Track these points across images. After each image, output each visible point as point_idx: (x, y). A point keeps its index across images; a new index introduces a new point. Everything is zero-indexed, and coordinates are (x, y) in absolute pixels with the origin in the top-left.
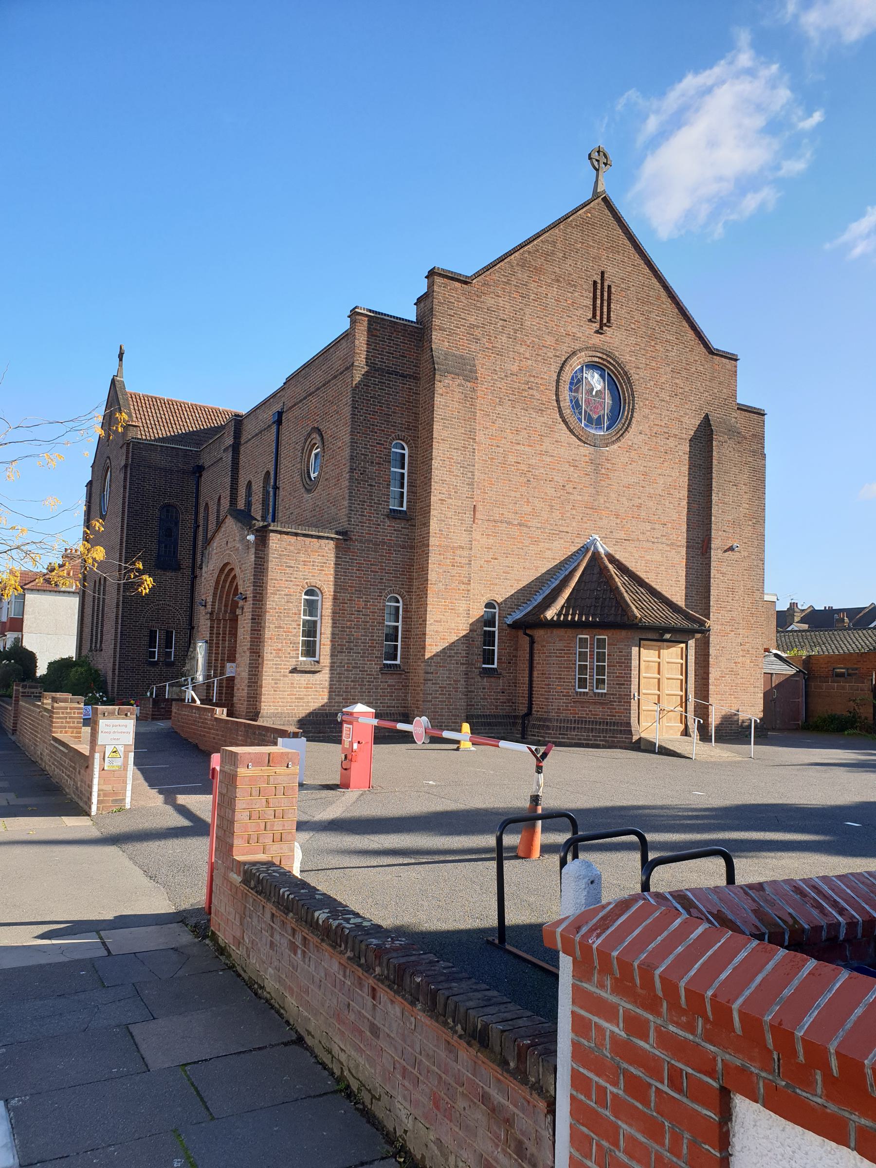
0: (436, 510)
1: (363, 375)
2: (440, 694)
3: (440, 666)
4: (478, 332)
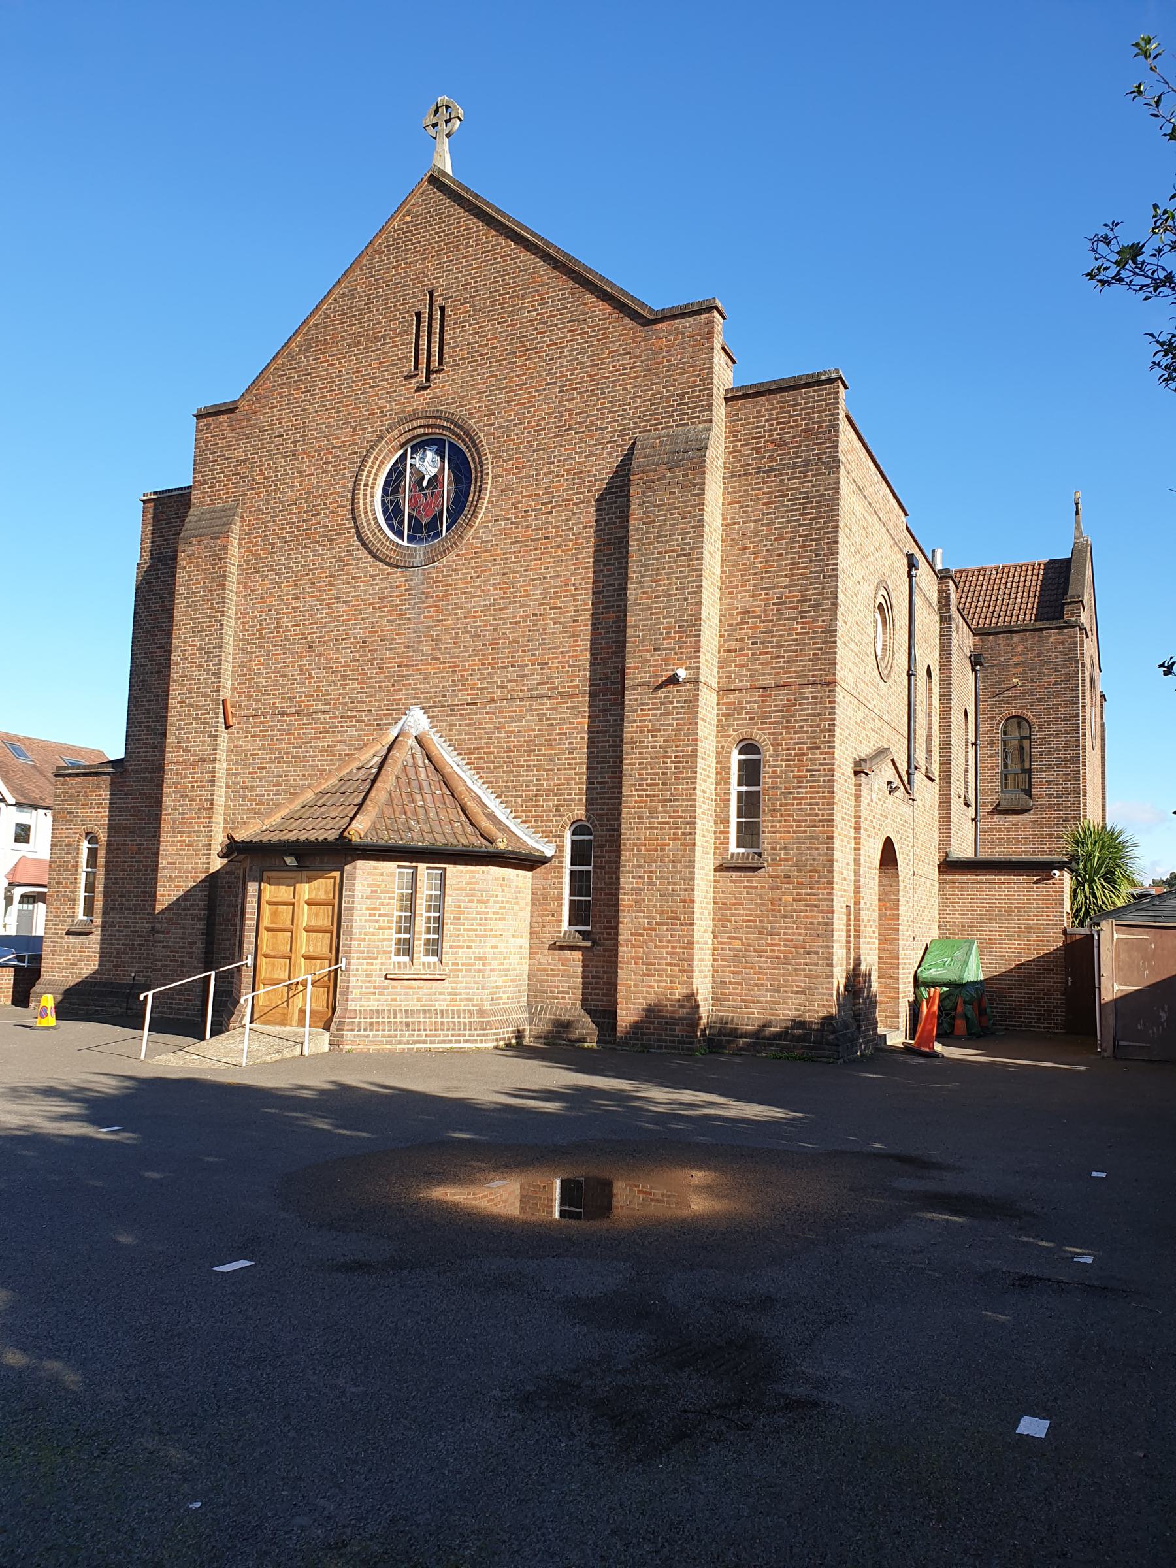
0: (175, 716)
1: (146, 572)
2: (171, 961)
3: (173, 924)
4: (245, 468)
